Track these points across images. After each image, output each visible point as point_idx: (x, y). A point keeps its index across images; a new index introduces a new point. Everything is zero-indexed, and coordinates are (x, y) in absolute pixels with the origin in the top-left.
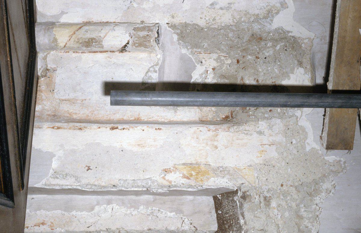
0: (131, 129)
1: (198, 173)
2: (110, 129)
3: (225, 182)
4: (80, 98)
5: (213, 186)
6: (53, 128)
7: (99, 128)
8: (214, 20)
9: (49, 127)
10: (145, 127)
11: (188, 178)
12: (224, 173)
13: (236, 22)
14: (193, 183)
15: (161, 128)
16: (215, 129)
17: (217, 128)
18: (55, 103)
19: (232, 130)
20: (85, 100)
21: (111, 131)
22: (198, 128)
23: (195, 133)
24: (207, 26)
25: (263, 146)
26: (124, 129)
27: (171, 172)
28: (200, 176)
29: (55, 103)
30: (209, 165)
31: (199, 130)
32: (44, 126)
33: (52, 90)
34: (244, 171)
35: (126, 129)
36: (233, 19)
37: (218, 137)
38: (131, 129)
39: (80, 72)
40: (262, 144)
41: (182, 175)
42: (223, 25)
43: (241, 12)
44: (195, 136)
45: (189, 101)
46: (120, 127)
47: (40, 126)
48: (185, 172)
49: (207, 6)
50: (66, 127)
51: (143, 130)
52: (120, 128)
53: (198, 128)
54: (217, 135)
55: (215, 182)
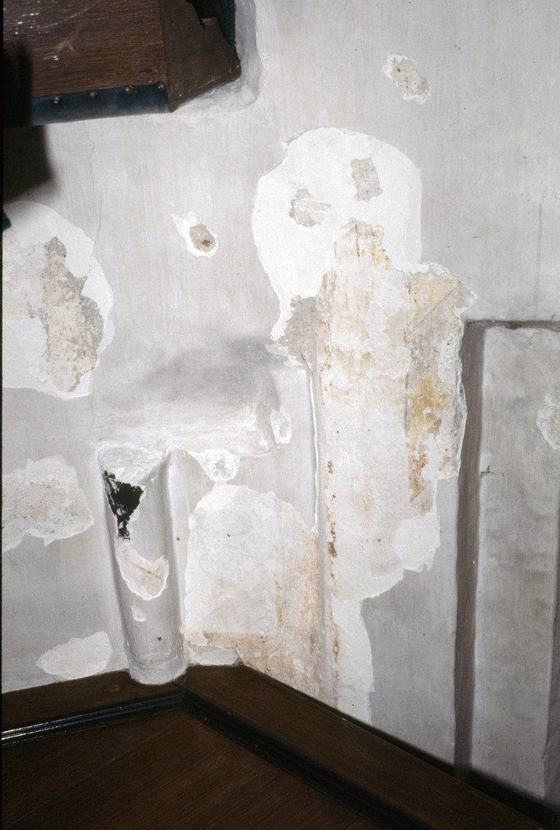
0: (333, 519)
3: (448, 347)
4: (275, 592)
5: (457, 372)
6: (337, 653)
8: (74, 341)
11: (438, 423)
12: (427, 350)
13: (71, 293)
14: (447, 416)
15: (329, 462)
16: (324, 354)
17: (322, 348)
22: (323, 388)
23: (334, 396)
24: (90, 354)
25: (361, 251)
26: (333, 533)
27: (424, 456)
28: (432, 399)
30: (408, 376)
35: (333, 528)
36: (67, 301)
37: (342, 349)
38: (333, 519)
39: (221, 593)
41: (432, 435)
42: (83, 320)
43: (47, 286)
50: (333, 633)
52: (331, 540)
53: (323, 388)
54: (338, 350)
55: (447, 369)
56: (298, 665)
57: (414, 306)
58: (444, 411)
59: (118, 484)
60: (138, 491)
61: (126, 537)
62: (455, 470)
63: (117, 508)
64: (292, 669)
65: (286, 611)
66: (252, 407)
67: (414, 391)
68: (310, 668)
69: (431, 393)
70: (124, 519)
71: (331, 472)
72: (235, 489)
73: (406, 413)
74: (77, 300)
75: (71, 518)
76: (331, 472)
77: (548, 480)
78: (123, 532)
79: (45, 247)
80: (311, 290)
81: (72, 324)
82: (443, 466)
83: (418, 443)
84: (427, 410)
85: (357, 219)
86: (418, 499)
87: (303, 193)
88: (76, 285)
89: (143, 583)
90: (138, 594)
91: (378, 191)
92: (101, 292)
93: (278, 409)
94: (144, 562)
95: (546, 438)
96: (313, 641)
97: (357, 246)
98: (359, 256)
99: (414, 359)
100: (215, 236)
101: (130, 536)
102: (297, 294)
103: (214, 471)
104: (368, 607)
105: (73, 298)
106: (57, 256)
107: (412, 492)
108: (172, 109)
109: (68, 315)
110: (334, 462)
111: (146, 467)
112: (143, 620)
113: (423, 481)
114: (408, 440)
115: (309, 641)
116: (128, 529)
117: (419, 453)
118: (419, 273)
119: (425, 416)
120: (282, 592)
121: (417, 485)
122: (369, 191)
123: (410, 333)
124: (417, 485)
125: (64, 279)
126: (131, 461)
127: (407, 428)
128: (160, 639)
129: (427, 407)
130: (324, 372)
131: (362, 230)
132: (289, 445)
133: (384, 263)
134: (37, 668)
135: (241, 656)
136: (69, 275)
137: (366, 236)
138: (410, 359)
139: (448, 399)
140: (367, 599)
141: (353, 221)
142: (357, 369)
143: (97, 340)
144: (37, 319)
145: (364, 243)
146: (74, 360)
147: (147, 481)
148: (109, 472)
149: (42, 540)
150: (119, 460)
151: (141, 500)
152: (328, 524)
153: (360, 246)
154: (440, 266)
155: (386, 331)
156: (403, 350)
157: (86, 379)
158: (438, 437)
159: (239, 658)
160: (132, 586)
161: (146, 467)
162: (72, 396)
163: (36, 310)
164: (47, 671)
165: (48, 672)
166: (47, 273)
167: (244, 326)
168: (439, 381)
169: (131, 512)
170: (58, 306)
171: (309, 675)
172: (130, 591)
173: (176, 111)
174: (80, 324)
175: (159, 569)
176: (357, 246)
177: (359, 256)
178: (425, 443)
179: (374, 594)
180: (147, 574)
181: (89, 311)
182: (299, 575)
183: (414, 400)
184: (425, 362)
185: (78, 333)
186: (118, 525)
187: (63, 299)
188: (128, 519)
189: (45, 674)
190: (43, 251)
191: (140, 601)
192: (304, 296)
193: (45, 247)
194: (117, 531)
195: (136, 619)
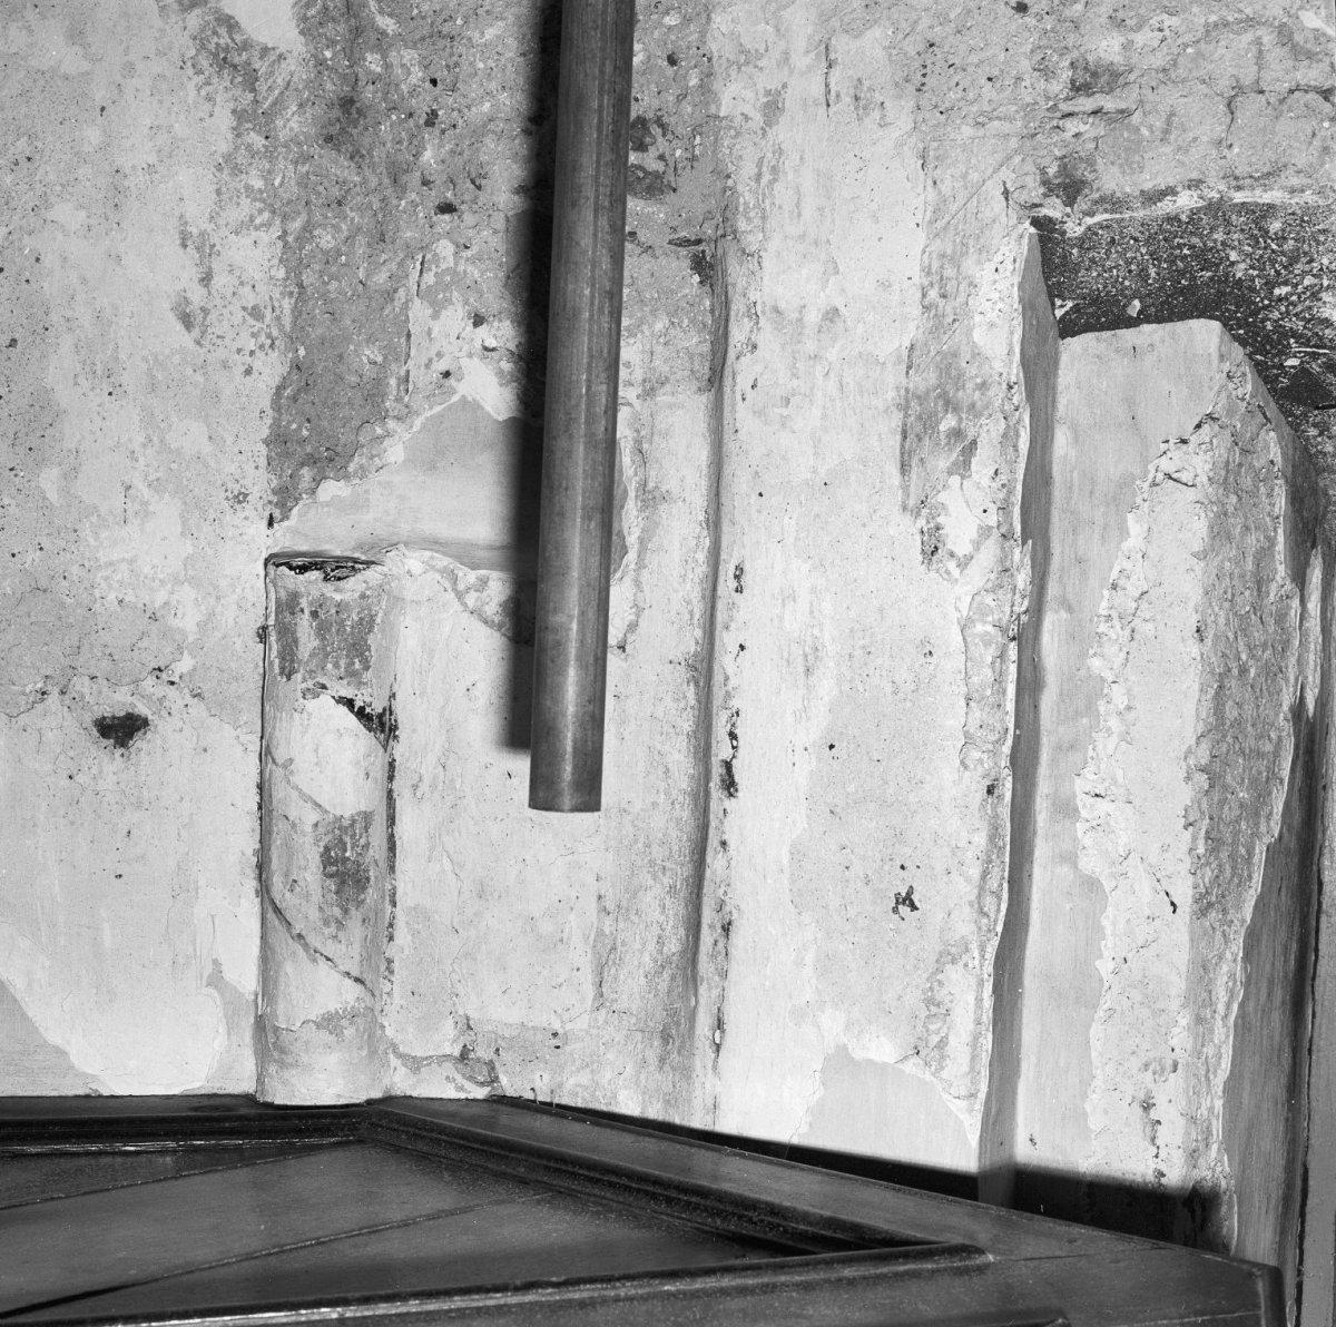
0: (735, 703)
1: (947, 403)
2: (731, 795)
3: (997, 276)
6: (718, 1047)
7: (724, 844)
8: (256, 313)
9: (715, 1068)
12: (954, 282)
14: (989, 432)
16: (746, 320)
19: (752, 241)
20: (600, 897)
21: (740, 794)
22: (739, 397)
24: (282, 347)
26: (733, 736)
31: (750, 394)
33: (555, 1042)
35: (733, 725)
37: (782, 305)
38: (735, 703)
46: (722, 750)
47: (710, 1102)
49: (191, 345)
50: (715, 992)
51: (742, 647)
54: (776, 310)
58: (983, 421)
65: (613, 971)
67: (925, 380)
69: (959, 382)
71: (739, 590)
84: (948, 422)
98: (828, 105)
99: (926, 308)
105: (268, 225)
110: (747, 567)
117: (928, 522)
119: (942, 436)
120: (608, 921)
129: (949, 416)
133: (876, 114)
138: (916, 311)
163: (195, 231)
168: (976, 354)
170: (237, 234)
177: (828, 105)
184: (949, 310)
185: (267, 298)
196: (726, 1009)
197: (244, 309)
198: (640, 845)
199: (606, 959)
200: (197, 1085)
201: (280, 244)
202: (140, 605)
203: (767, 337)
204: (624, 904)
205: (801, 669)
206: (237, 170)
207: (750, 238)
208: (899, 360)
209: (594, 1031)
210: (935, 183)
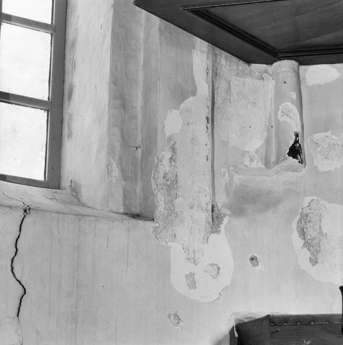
0: (207, 134)
1: (169, 187)
2: (207, 117)
6: (207, 69)
7: (208, 108)
8: (310, 221)
9: (208, 65)
10: (209, 146)
11: (164, 177)
13: (309, 242)
18: (227, 77)
19: (207, 226)
20: (230, 102)
21: (205, 117)
22: (209, 194)
23: (205, 190)
25: (193, 252)
26: (207, 128)
27: (170, 163)
29: (227, 77)
30: (176, 198)
31: (207, 194)
32: (209, 62)
33: (238, 75)
34: (171, 229)
37: (201, 211)
38: (207, 134)
40: (195, 251)
42: (305, 230)
44: (201, 190)
45: (275, 123)
46: (209, 125)
47: (209, 59)
48: (169, 175)
49: (322, 213)
51: (206, 145)
52: (208, 125)
56: (223, 62)
57: (174, 228)
59: (297, 159)
60: (289, 154)
61: (296, 133)
62: (158, 156)
63: (299, 147)
64: (226, 59)
65: (227, 88)
66: (236, 184)
67: (173, 192)
68: (218, 60)
70: (296, 142)
71: (207, 156)
72: (247, 149)
73: (177, 182)
74: (307, 239)
75: (318, 142)
76: (207, 156)
77: (113, 144)
78: (297, 135)
79: (318, 263)
80: (213, 236)
81: (309, 229)
82: (162, 158)
83: (172, 169)
84: (169, 183)
85: (194, 265)
86: (173, 143)
87: (214, 277)
88: (307, 245)
89: (290, 111)
90: (293, 106)
91: (186, 276)
92: (297, 241)
93: (226, 184)
94: (288, 119)
95: (114, 163)
96: (216, 73)
97: (194, 254)
99: (173, 206)
100: (249, 262)
101: (294, 133)
102: (218, 235)
103: (254, 158)
104: (194, 93)
106: (313, 258)
107: (176, 147)
108: (269, 315)
109: (311, 233)
111: (285, 165)
112: (292, 93)
113: (171, 151)
114: (177, 170)
115: (218, 73)
116: (295, 137)
118: (171, 242)
121: (173, 149)
122: (191, 277)
123: (175, 217)
124: (173, 149)
125: (311, 248)
126: (291, 167)
127: (177, 175)
128: (285, 83)
130: (209, 202)
131: (192, 261)
132: (222, 167)
133: (185, 247)
134: (340, 72)
135: (248, 67)
136: (309, 250)
137: (191, 259)
139: (161, 187)
140: (194, 96)
141: (196, 265)
142: (196, 202)
143: (300, 221)
144: (324, 233)
145: (192, 255)
146: (310, 213)
147: (285, 159)
148: (301, 164)
149: (332, 134)
150: (295, 168)
151: (289, 150)
152: (209, 132)
153: (193, 254)
154: (164, 244)
155: (184, 218)
156: (178, 209)
157: (306, 204)
158: (164, 171)
159: (249, 66)
160: (295, 110)
161: (285, 165)
162: (314, 197)
164: (335, 70)
165: (335, 70)
166: (318, 252)
167: (239, 223)
169: (293, 145)
171: (219, 56)
172: (296, 107)
173: (267, 315)
174: (307, 228)
175: (283, 116)
176: (194, 254)
178: (170, 169)
179: (191, 98)
180: (288, 114)
181: (303, 233)
182: (220, 105)
183: (174, 188)
184: (170, 204)
186: (299, 139)
187: (312, 240)
188: (294, 142)
189: (337, 69)
190: (319, 261)
191: (292, 103)
192: (215, 234)
193: (318, 263)
194: (299, 136)
195: (295, 94)
196: (206, 76)
197: (312, 222)
198: (222, 112)
199: (228, 90)
200: (311, 67)
201: (305, 236)
202: (329, 160)
203: (204, 205)
204: (225, 101)
205: (195, 139)
206: (316, 251)
207: (208, 226)
208: (179, 196)
209: (230, 76)
210: (173, 230)
